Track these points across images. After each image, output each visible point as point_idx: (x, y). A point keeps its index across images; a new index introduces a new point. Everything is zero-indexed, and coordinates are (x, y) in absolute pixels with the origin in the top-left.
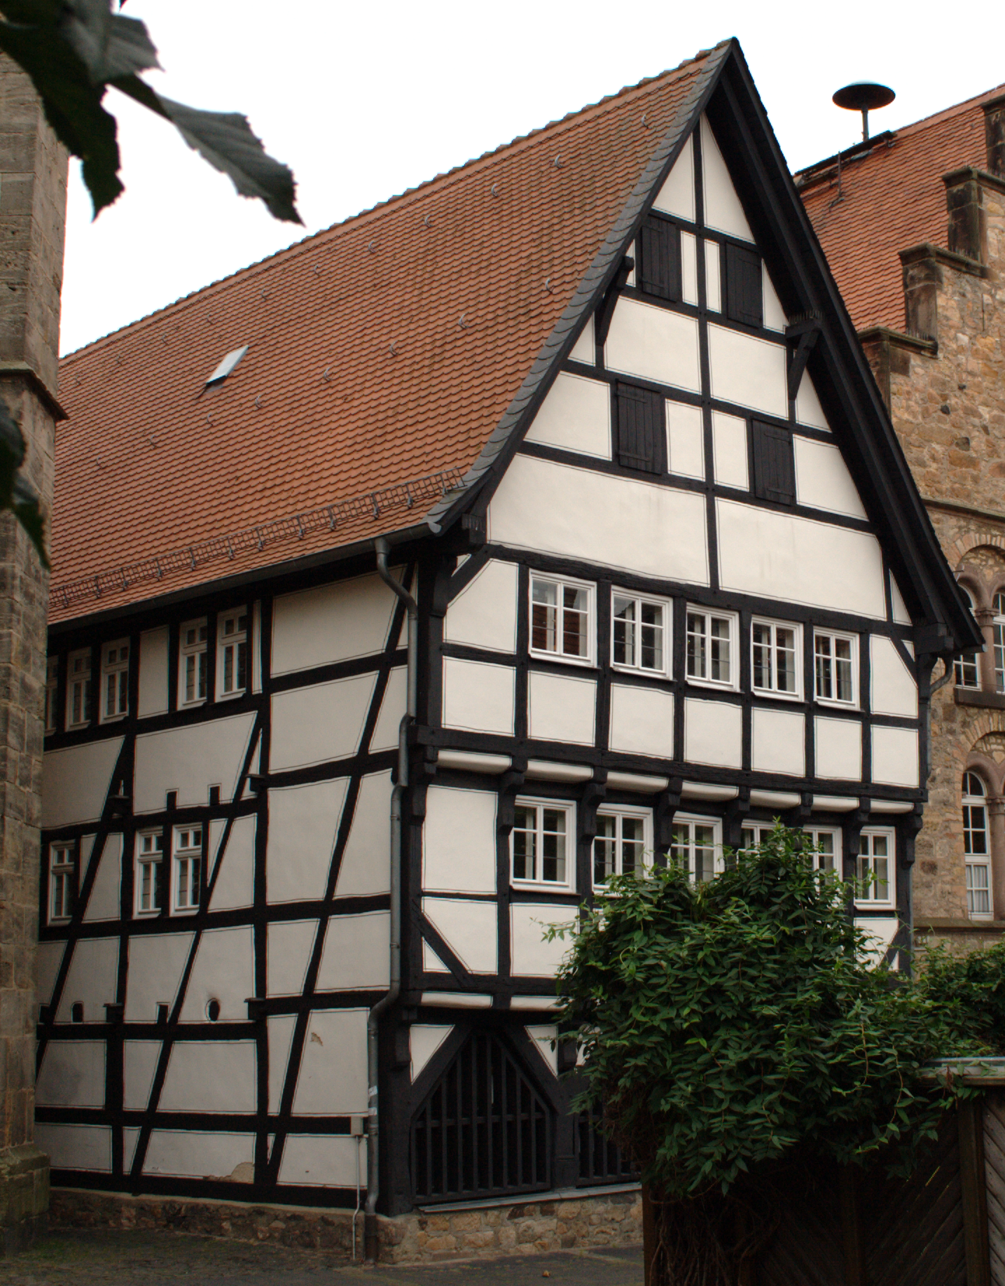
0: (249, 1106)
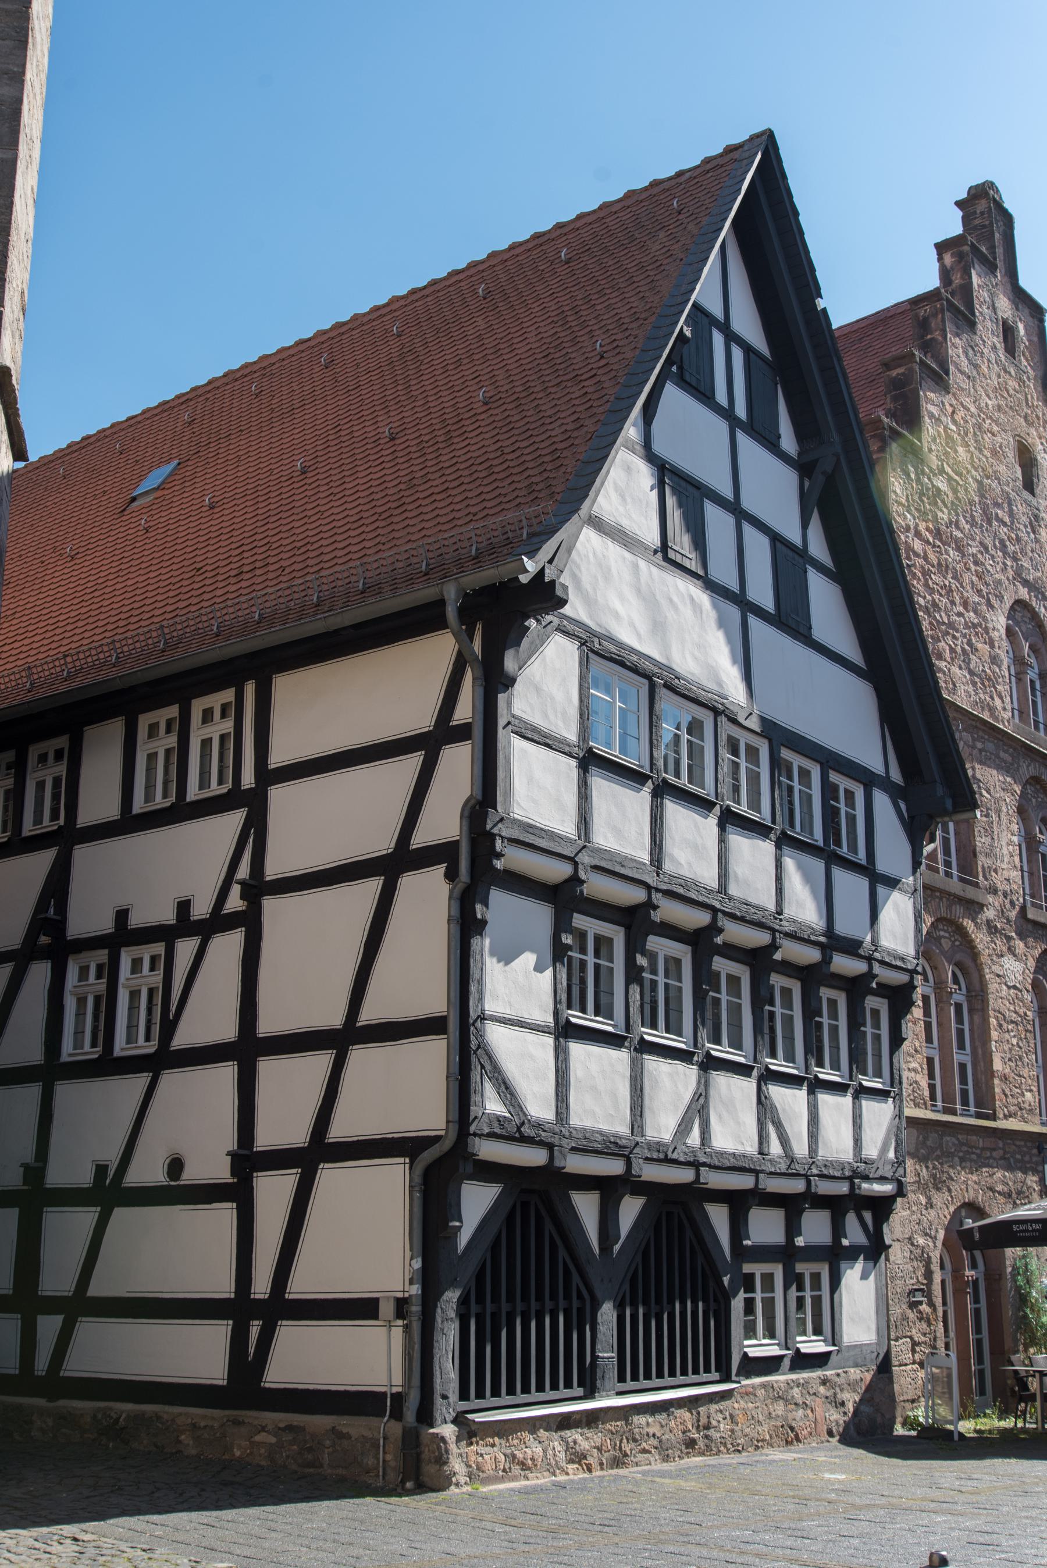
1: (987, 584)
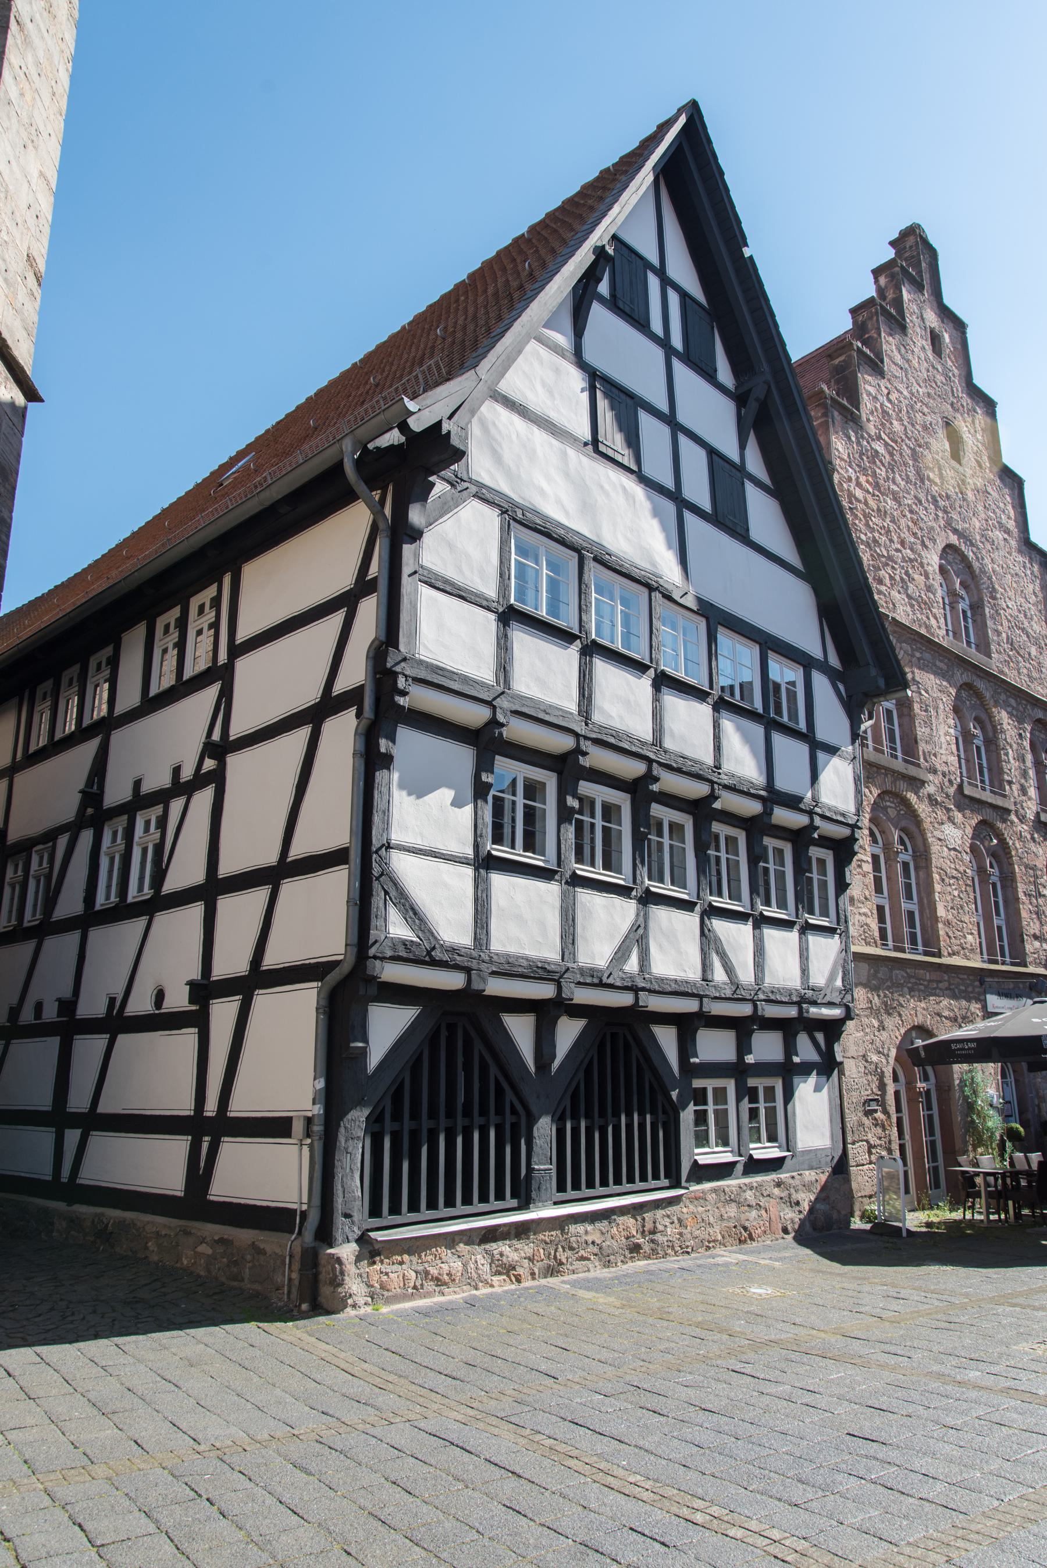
0: (183, 1105)
1: (921, 529)
